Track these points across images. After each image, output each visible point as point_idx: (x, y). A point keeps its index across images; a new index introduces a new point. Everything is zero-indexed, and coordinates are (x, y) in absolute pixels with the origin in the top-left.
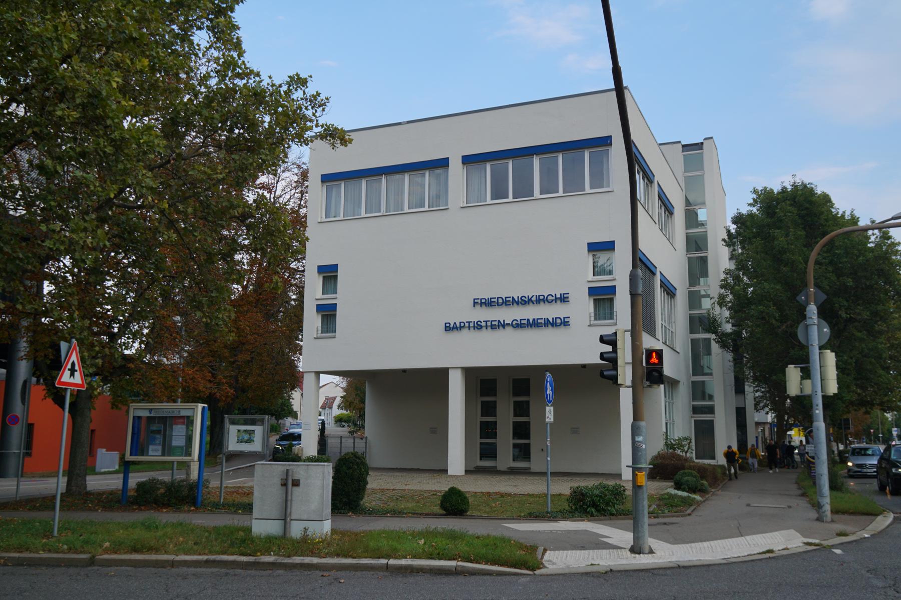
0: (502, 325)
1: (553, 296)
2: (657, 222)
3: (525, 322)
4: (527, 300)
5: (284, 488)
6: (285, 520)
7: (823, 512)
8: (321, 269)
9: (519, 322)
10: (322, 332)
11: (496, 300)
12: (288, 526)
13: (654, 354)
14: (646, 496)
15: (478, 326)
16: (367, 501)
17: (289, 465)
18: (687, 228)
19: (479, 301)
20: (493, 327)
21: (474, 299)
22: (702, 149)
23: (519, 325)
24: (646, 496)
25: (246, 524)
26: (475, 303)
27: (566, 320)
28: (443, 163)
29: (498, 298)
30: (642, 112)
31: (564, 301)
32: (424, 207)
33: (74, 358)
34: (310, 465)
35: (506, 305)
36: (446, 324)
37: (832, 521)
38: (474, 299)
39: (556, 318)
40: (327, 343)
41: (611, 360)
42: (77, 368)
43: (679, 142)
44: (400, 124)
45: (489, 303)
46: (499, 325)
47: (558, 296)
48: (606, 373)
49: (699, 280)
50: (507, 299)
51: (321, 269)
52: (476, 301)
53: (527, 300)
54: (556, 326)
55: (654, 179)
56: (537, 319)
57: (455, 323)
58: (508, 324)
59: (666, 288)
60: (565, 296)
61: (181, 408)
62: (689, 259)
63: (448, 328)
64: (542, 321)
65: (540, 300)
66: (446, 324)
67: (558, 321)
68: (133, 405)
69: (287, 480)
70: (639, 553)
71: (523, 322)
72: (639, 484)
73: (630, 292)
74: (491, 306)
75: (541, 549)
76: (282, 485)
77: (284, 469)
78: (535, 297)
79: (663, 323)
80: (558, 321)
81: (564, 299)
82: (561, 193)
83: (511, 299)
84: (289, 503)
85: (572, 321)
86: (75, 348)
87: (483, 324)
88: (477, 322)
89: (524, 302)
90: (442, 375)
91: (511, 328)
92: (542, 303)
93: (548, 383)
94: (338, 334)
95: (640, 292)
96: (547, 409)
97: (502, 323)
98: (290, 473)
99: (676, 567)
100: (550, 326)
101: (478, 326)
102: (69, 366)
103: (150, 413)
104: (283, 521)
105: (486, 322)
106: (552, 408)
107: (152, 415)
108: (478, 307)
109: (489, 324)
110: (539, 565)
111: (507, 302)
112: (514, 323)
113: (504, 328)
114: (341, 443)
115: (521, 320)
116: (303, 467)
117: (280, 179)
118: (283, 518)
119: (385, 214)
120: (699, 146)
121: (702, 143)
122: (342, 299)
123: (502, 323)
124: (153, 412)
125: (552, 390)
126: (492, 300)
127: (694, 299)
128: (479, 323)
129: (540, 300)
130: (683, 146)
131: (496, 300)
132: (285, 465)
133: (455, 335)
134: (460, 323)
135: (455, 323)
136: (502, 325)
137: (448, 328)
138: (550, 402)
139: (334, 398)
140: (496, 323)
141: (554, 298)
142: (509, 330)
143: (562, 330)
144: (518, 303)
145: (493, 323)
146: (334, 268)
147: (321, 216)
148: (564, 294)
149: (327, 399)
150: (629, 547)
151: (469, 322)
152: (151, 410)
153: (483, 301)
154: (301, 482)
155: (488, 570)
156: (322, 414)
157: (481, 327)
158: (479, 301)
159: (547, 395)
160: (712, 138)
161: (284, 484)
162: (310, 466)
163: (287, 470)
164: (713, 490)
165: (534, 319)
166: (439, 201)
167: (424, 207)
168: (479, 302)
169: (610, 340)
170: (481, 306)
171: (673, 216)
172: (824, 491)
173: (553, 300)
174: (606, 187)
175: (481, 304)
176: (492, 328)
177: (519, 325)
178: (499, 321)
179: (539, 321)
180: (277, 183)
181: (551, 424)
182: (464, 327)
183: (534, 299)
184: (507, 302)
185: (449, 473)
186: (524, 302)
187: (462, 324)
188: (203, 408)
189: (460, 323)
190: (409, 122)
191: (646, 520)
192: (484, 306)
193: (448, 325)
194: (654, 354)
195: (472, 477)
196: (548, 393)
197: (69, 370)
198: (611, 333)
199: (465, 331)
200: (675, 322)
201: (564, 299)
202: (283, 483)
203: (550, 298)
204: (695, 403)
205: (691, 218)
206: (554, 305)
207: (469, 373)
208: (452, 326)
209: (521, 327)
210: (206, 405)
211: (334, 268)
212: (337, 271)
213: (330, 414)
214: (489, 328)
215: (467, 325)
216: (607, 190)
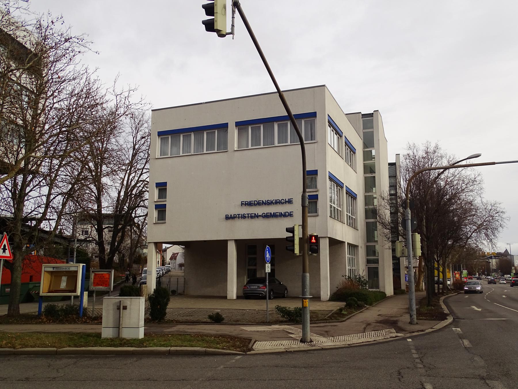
0: (256, 216)
1: (284, 200)
2: (344, 158)
3: (269, 214)
4: (270, 202)
5: (118, 311)
6: (119, 328)
7: (413, 319)
8: (158, 185)
9: (266, 215)
10: (158, 220)
11: (253, 202)
12: (120, 331)
13: (313, 238)
14: (308, 312)
15: (243, 217)
16: (168, 317)
17: (121, 298)
18: (364, 161)
19: (244, 203)
20: (252, 217)
21: (242, 202)
22: (373, 117)
23: (267, 216)
24: (308, 312)
25: (98, 331)
26: (242, 204)
27: (291, 213)
28: (224, 127)
29: (255, 201)
30: (335, 99)
31: (290, 203)
32: (214, 150)
33: (5, 242)
34: (132, 298)
35: (259, 205)
36: (226, 215)
37: (417, 323)
38: (242, 202)
39: (286, 212)
40: (161, 227)
41: (291, 240)
42: (7, 248)
43: (360, 113)
44: (201, 103)
45: (249, 204)
46: (255, 216)
47: (287, 200)
48: (288, 248)
49: (373, 189)
50: (260, 202)
51: (158, 185)
52: (243, 203)
53: (270, 202)
54: (286, 216)
55: (342, 135)
56: (276, 213)
57: (231, 215)
58: (260, 216)
59: (350, 194)
60: (291, 200)
61: (72, 266)
62: (365, 177)
63: (228, 218)
64: (278, 214)
65: (278, 202)
66: (226, 215)
67: (287, 214)
68: (44, 265)
69: (120, 306)
70: (304, 343)
71: (268, 214)
72: (305, 306)
73: (302, 205)
74: (251, 205)
75: (253, 342)
76: (117, 309)
77: (118, 300)
78: (274, 200)
79: (348, 214)
80: (287, 214)
81: (290, 202)
82: (289, 143)
83: (261, 202)
84: (121, 319)
85: (294, 214)
86: (6, 237)
87: (247, 216)
88: (243, 214)
89: (269, 203)
90: (223, 244)
91: (261, 218)
92: (278, 204)
93: (267, 251)
94: (167, 221)
95: (307, 205)
96: (267, 265)
97: (257, 215)
98: (122, 303)
99: (321, 349)
100: (282, 217)
101: (243, 217)
102: (2, 247)
103: (53, 269)
104: (118, 328)
105: (248, 214)
106: (270, 265)
107: (54, 270)
108: (244, 206)
109: (250, 215)
110: (251, 349)
111: (259, 203)
112: (263, 215)
113: (258, 218)
114: (178, 282)
115: (267, 213)
116: (129, 299)
117: (139, 131)
118: (118, 327)
119: (193, 154)
120: (371, 115)
121: (373, 113)
122: (169, 202)
123: (257, 215)
124: (55, 268)
125: (270, 255)
126: (251, 202)
127: (368, 200)
128: (244, 215)
129: (278, 202)
130: (362, 115)
131: (253, 202)
132: (119, 298)
133: (230, 222)
134: (234, 215)
135: (231, 215)
136: (256, 216)
137: (228, 218)
138: (268, 262)
139: (178, 253)
140: (254, 215)
141: (285, 201)
142: (261, 218)
143: (289, 218)
144: (265, 204)
145: (252, 215)
146: (165, 184)
147: (158, 155)
148: (290, 199)
149: (174, 254)
150: (300, 339)
151: (239, 215)
152: (54, 268)
153: (247, 203)
154: (128, 307)
155: (225, 352)
156: (171, 264)
157: (245, 217)
158: (244, 203)
159: (266, 258)
160: (378, 111)
161: (119, 308)
162: (132, 299)
163: (120, 301)
164: (368, 306)
165: (274, 213)
166: (223, 146)
167: (214, 150)
168: (244, 203)
169: (291, 230)
170: (245, 205)
171: (355, 154)
172: (413, 308)
173: (284, 202)
174: (314, 140)
175: (246, 204)
176: (251, 218)
177: (267, 216)
178: (255, 214)
179: (277, 214)
180: (137, 133)
181: (269, 273)
182: (236, 217)
183: (274, 201)
184: (259, 203)
185: (228, 298)
186: (269, 203)
187: (235, 216)
188: (83, 266)
189: (234, 215)
190: (206, 103)
191: (309, 325)
192: (247, 205)
193: (227, 216)
194: (313, 238)
195: (240, 301)
196: (267, 256)
197: (2, 249)
198: (292, 227)
199: (236, 219)
200: (356, 213)
201: (290, 202)
202: (118, 308)
203: (283, 201)
204: (369, 258)
205: (368, 156)
206: (284, 205)
207: (239, 243)
208: (229, 216)
209: (267, 217)
210: (85, 264)
211: (165, 184)
212: (166, 186)
213: (175, 263)
214: (250, 218)
215: (238, 216)
216: (311, 142)
